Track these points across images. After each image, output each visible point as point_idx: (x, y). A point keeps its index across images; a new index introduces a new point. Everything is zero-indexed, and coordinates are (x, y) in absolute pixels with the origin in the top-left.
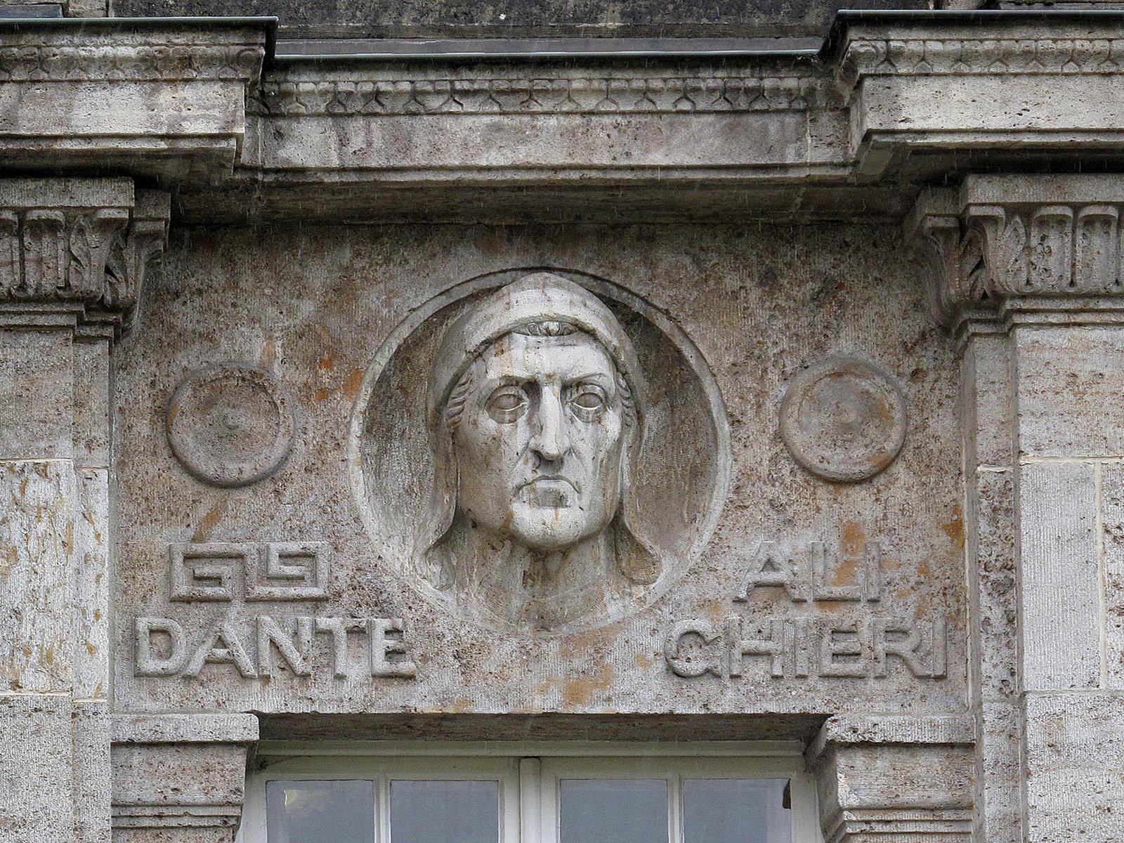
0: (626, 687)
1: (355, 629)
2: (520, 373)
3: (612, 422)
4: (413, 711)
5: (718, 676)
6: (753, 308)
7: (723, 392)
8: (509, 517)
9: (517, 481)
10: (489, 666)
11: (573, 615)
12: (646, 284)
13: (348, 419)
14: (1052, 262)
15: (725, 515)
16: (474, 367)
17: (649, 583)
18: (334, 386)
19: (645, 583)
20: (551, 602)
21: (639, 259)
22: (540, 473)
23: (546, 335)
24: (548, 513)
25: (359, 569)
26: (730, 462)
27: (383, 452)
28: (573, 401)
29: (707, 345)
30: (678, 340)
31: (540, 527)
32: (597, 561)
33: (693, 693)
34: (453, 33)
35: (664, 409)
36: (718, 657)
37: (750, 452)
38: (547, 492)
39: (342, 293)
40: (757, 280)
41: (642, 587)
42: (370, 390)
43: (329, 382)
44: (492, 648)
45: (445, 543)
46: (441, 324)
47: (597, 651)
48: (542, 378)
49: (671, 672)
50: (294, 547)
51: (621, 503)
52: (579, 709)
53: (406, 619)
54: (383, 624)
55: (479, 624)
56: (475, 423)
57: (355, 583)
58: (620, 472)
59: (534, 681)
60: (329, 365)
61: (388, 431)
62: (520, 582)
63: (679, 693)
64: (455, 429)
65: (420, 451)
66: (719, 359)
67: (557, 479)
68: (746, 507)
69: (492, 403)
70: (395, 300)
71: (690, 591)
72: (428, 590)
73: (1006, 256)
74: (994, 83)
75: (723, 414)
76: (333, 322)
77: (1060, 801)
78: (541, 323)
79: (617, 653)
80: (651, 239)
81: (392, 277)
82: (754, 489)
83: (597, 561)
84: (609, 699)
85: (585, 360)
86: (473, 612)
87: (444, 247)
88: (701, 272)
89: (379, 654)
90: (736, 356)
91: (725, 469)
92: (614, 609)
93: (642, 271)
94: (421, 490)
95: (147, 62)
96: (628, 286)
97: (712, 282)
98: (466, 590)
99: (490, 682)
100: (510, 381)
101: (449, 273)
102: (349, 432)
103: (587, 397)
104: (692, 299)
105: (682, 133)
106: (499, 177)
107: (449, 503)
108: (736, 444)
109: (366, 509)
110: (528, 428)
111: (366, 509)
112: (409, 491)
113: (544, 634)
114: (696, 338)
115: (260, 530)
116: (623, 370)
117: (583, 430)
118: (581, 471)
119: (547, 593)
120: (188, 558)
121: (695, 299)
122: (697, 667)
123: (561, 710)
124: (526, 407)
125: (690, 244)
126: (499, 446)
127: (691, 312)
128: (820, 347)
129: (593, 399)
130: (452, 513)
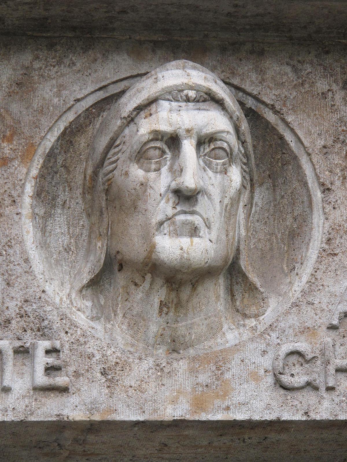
0: (241, 398)
1: (21, 349)
2: (165, 127)
3: (235, 175)
4: (66, 419)
5: (316, 389)
6: (338, 106)
7: (317, 167)
8: (152, 248)
9: (160, 217)
10: (130, 380)
11: (199, 340)
12: (257, 86)
13: (23, 182)
15: (319, 260)
16: (127, 131)
17: (259, 316)
18: (13, 156)
19: (256, 316)
20: (182, 327)
21: (251, 67)
22: (179, 208)
23: (185, 101)
24: (185, 241)
25: (26, 301)
26: (322, 221)
27: (48, 216)
28: (205, 155)
29: (305, 132)
30: (282, 129)
31: (178, 252)
32: (218, 297)
33: (296, 403)
35: (267, 189)
36: (317, 372)
37: (338, 212)
38: (184, 223)
40: (341, 85)
41: (253, 320)
42: (41, 161)
43: (9, 153)
44: (133, 365)
45: (95, 284)
46: (98, 116)
47: (218, 369)
48: (182, 133)
49: (278, 386)
51: (238, 250)
52: (204, 417)
53: (61, 341)
54: (44, 344)
55: (122, 347)
56: (127, 174)
57: (22, 312)
58: (237, 225)
59: (167, 393)
60: (10, 140)
61: (53, 199)
62: (157, 311)
63: (285, 403)
64: (109, 185)
65: (77, 218)
66: (313, 143)
67: (193, 213)
68: (335, 255)
69: (141, 156)
70: (64, 92)
71: (293, 320)
72: (82, 319)
75: (316, 184)
76: (15, 107)
78: (182, 91)
79: (234, 370)
80: (261, 53)
81: (62, 75)
82: (342, 241)
83: (218, 297)
84: (228, 408)
85: (215, 121)
86: (117, 337)
87: (104, 55)
88: (298, 78)
89: (40, 370)
90: (326, 140)
91: (319, 227)
92: (231, 336)
93: (254, 76)
94: (77, 249)
96: (243, 86)
97: (307, 86)
98: (112, 323)
99: (130, 394)
100: (157, 136)
101: (107, 73)
102: (23, 192)
103: (217, 151)
104: (292, 97)
107: (101, 248)
108: (328, 206)
109: (35, 255)
110: (170, 174)
111: (35, 255)
112: (67, 250)
113: (175, 355)
114: (295, 126)
116: (243, 139)
117: (213, 178)
118: (210, 209)
119: (179, 319)
121: (294, 98)
122: (300, 380)
123: (188, 417)
124: (168, 159)
125: (290, 58)
126: (145, 191)
127: (291, 107)
129: (221, 153)
130: (103, 257)
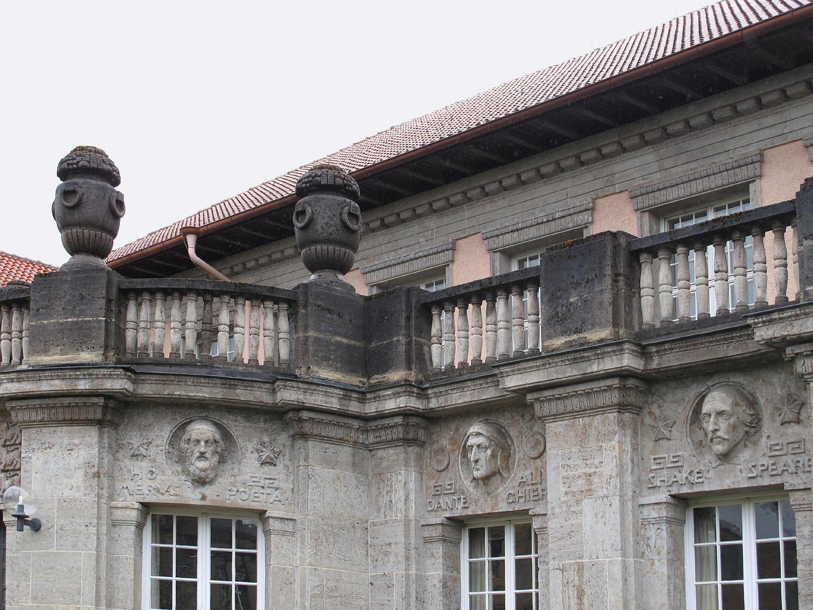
14: (545, 409)
34: (472, 373)
39: (457, 429)
50: (449, 483)
52: (493, 512)
73: (538, 410)
74: (520, 375)
77: (554, 526)
79: (499, 499)
89: (462, 503)
95: (394, 394)
105: (488, 392)
106: (677, 367)
115: (445, 480)
118: (483, 462)
120: (655, 459)
128: (532, 430)
